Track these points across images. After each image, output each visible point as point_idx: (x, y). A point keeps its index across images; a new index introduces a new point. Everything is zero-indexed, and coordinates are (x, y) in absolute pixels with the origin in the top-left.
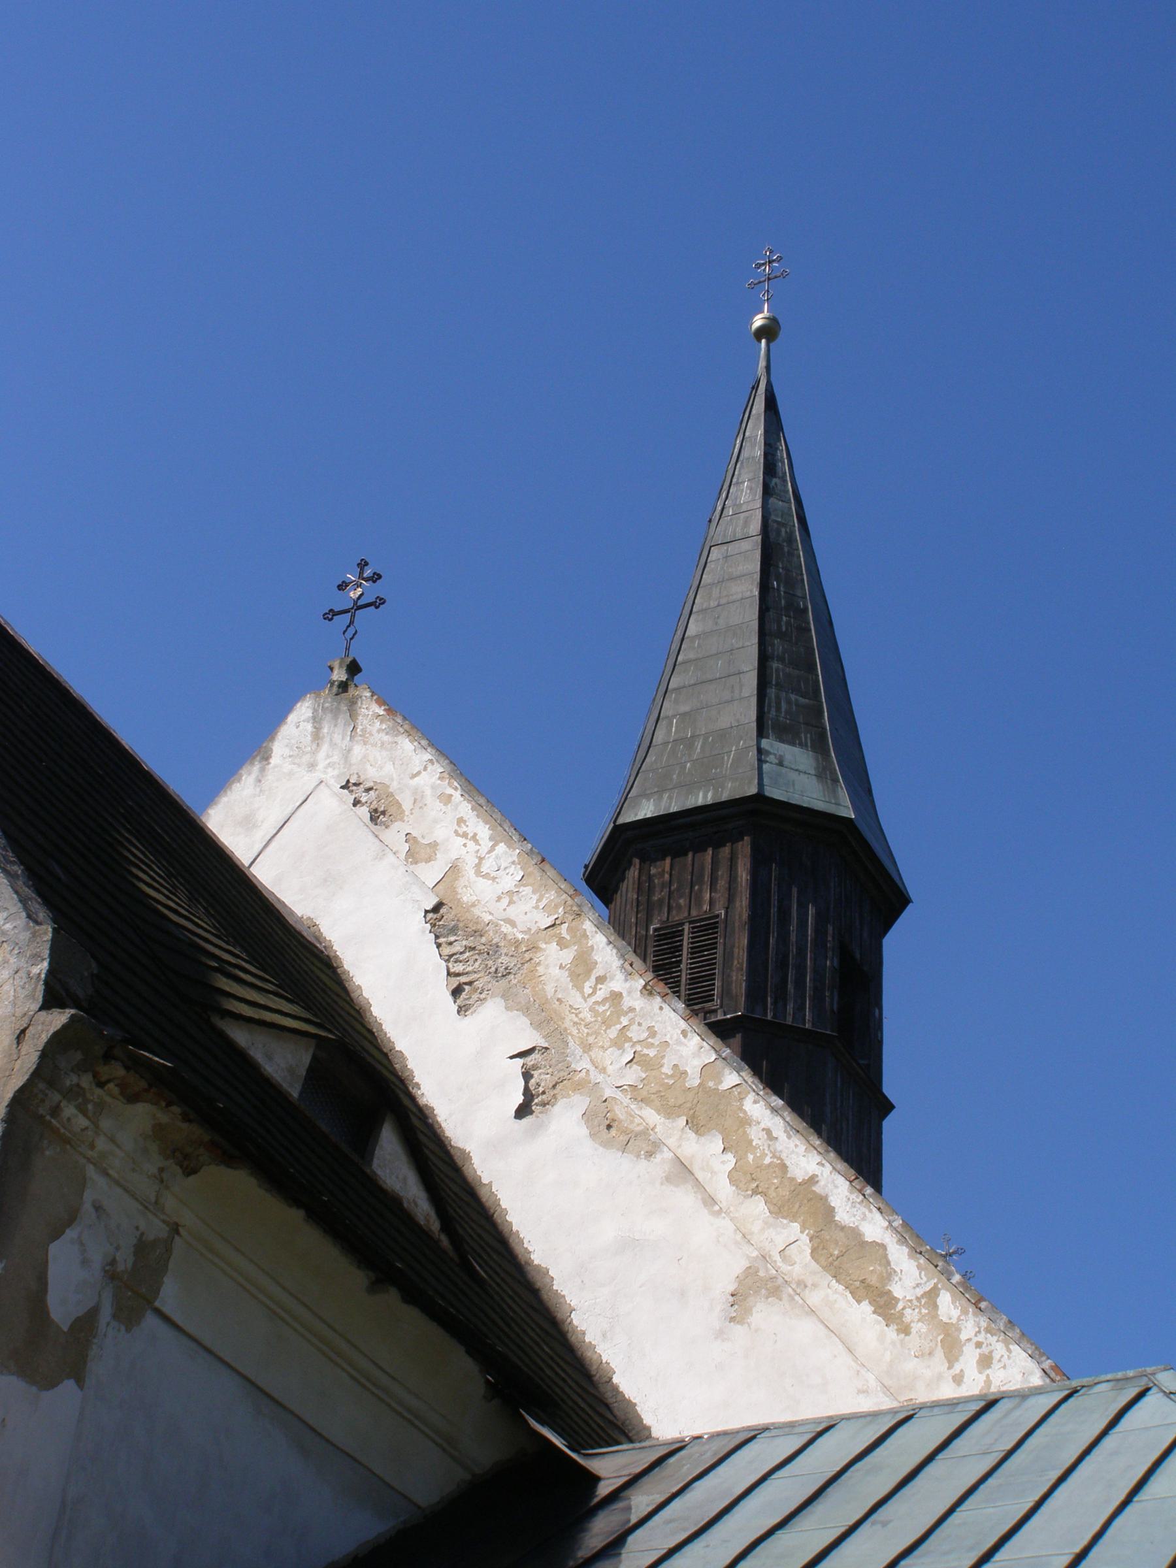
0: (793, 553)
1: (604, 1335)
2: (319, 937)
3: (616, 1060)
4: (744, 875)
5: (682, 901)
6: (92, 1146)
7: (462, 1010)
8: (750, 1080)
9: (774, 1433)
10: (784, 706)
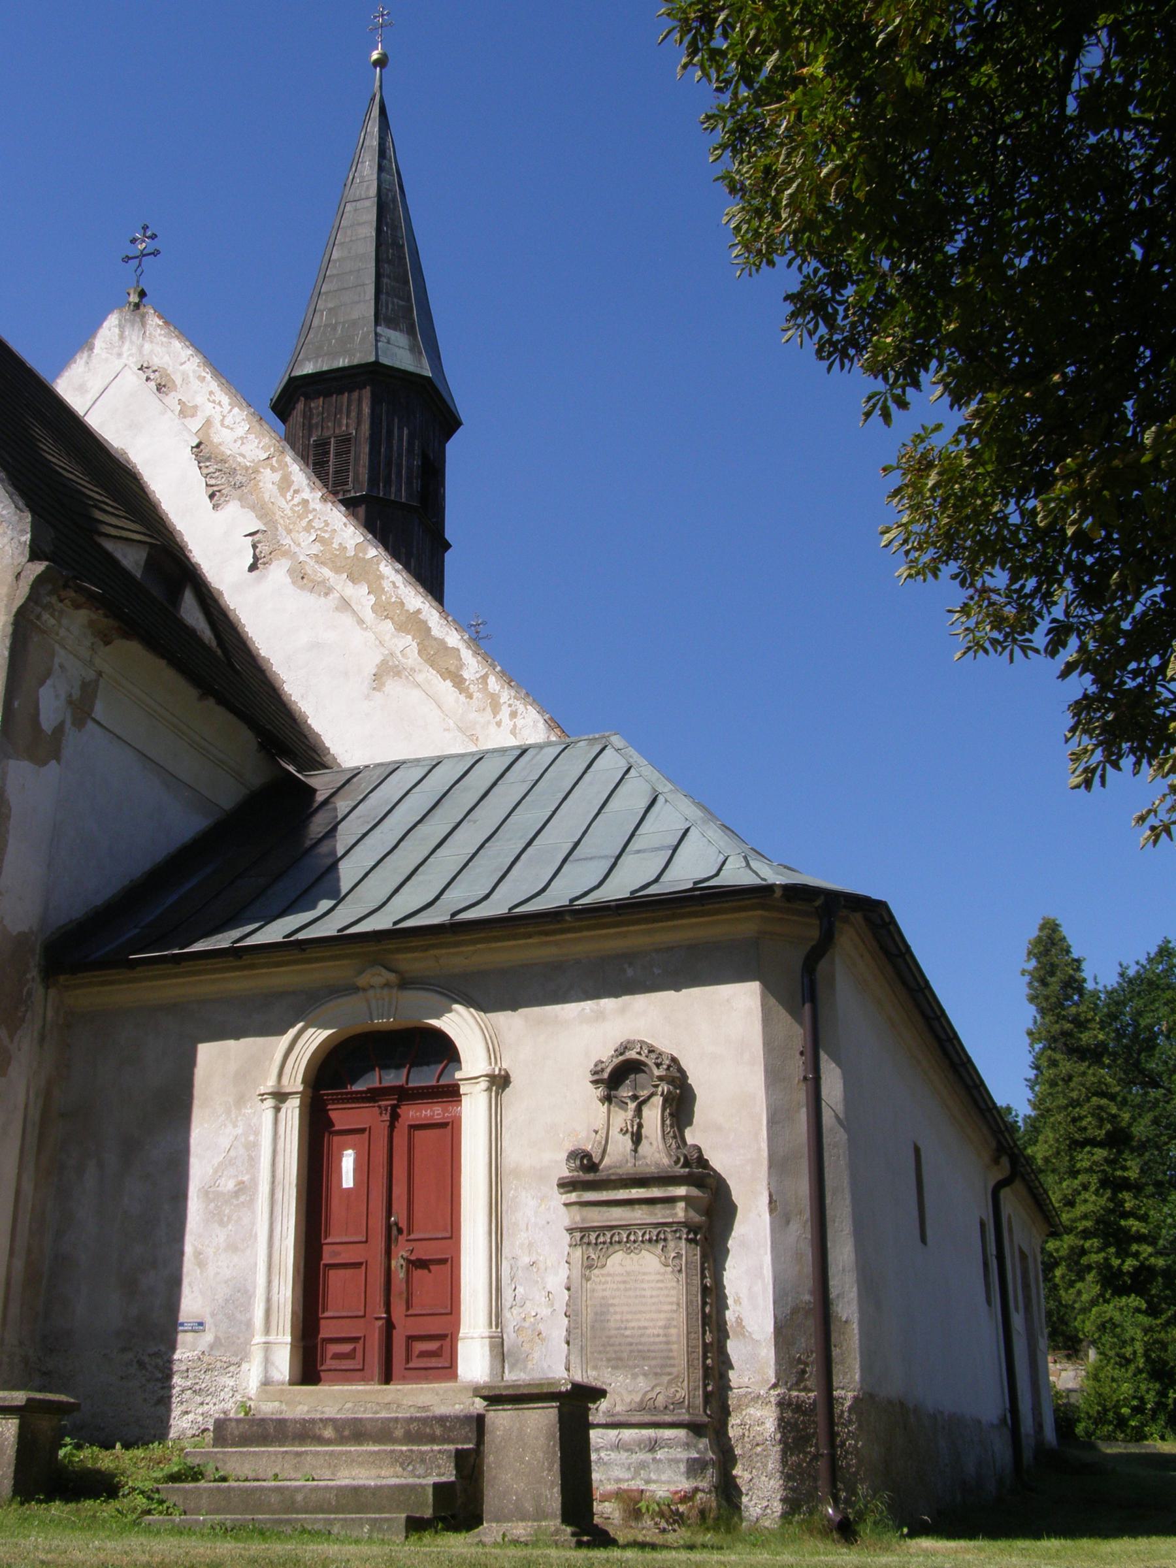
0: (396, 208)
1: (302, 697)
2: (128, 461)
3: (306, 539)
4: (366, 410)
5: (330, 424)
6: (57, 634)
7: (215, 507)
8: (383, 554)
9: (409, 765)
10: (390, 306)
